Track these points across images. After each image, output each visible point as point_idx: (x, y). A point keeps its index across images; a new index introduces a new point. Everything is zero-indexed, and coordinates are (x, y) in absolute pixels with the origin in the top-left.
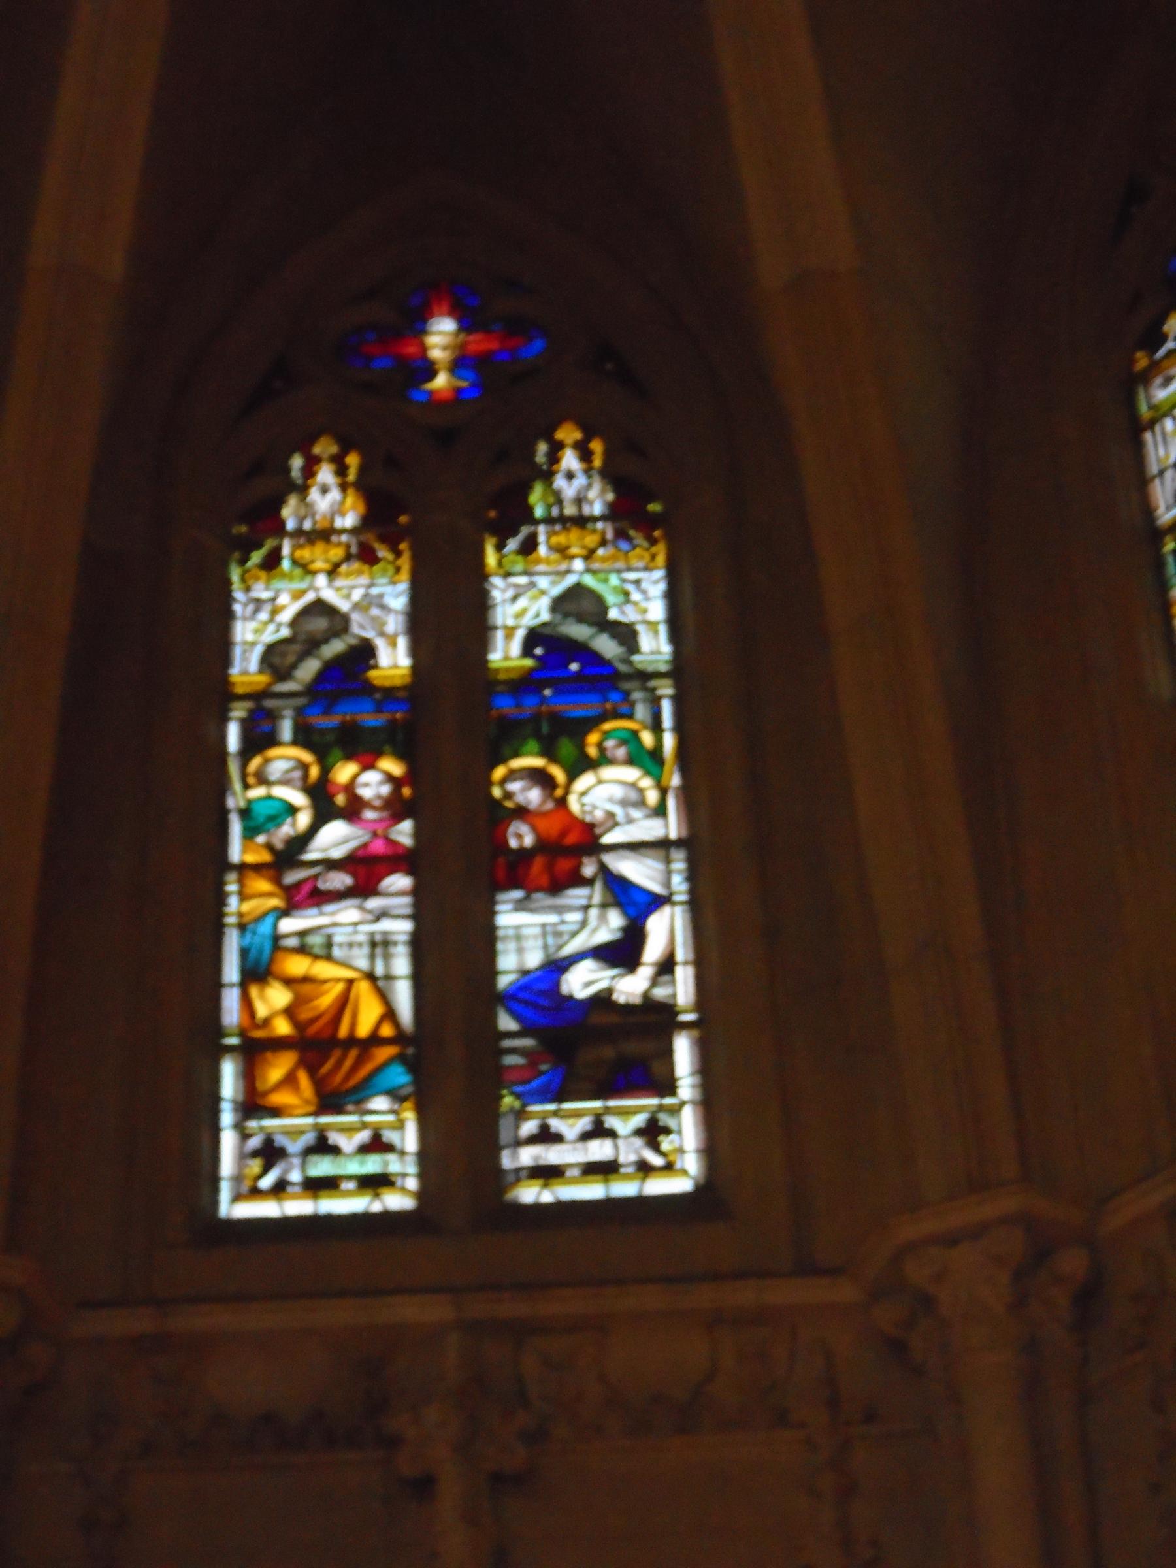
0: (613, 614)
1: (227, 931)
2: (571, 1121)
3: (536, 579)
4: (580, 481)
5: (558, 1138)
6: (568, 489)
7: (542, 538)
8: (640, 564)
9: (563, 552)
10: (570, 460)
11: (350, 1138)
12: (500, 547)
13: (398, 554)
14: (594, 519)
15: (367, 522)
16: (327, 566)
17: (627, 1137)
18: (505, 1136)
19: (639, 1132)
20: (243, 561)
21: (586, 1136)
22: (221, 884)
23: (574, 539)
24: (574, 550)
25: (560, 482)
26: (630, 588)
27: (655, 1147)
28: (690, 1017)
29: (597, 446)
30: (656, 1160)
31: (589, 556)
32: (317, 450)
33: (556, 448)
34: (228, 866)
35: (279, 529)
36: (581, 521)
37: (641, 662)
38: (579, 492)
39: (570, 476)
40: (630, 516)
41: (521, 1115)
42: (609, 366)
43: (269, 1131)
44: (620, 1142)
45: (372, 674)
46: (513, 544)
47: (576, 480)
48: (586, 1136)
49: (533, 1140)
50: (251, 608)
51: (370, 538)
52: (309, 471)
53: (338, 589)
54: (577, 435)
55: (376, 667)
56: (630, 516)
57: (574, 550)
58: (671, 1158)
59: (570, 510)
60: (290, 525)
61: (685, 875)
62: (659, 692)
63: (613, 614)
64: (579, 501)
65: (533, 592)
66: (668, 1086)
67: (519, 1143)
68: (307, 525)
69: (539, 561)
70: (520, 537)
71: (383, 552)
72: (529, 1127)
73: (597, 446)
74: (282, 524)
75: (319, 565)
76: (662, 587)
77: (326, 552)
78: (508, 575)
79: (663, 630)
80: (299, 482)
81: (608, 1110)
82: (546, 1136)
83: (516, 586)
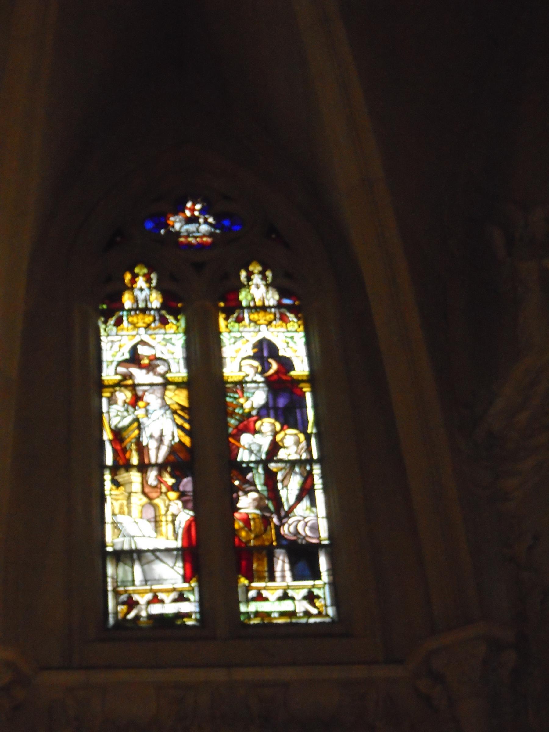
0: (281, 353)
1: (316, 491)
2: (297, 591)
3: (243, 334)
4: (146, 292)
5: (266, 599)
6: (141, 296)
7: (125, 319)
8: (172, 331)
9: (135, 326)
10: (141, 282)
11: (142, 597)
12: (226, 319)
13: (178, 320)
14: (270, 307)
15: (164, 306)
16: (145, 325)
17: (299, 600)
18: (241, 597)
19: (305, 598)
20: (105, 322)
21: (280, 599)
22: (103, 475)
23: (261, 317)
24: (262, 321)
25: (137, 292)
26: (289, 340)
27: (314, 605)
28: (326, 542)
29: (269, 274)
30: (314, 611)
31: (148, 327)
32: (137, 270)
33: (135, 276)
34: (319, 461)
35: (122, 308)
36: (145, 310)
37: (171, 377)
38: (146, 297)
39: (141, 290)
40: (170, 307)
41: (248, 589)
42: (274, 236)
43: (181, 589)
44: (296, 602)
45: (292, 373)
46: (112, 321)
47: (258, 290)
48: (280, 599)
49: (254, 599)
50: (110, 344)
51: (163, 312)
52: (133, 281)
53: (150, 335)
54: (145, 271)
55: (294, 369)
56: (170, 307)
57: (262, 321)
58: (321, 609)
59: (259, 303)
60: (244, 304)
61: (320, 475)
62: (304, 390)
63: (281, 353)
64: (146, 301)
65: (243, 340)
66: (317, 576)
67: (248, 601)
68: (252, 304)
69: (123, 329)
70: (235, 315)
71: (171, 319)
72: (252, 594)
73: (269, 274)
74: (240, 303)
75: (141, 324)
76: (303, 340)
77: (265, 316)
78: (230, 332)
79: (182, 362)
80: (129, 285)
81: (265, 588)
82: (260, 598)
83: (235, 338)
